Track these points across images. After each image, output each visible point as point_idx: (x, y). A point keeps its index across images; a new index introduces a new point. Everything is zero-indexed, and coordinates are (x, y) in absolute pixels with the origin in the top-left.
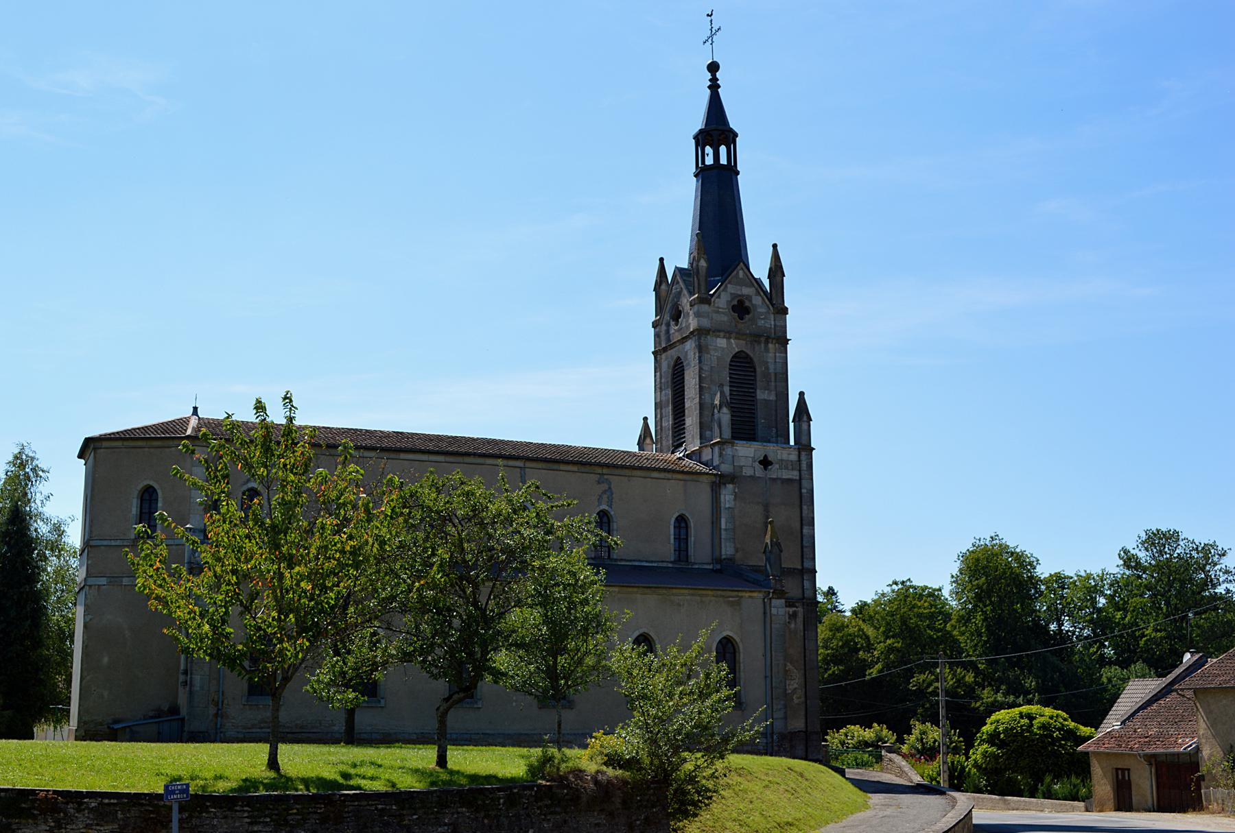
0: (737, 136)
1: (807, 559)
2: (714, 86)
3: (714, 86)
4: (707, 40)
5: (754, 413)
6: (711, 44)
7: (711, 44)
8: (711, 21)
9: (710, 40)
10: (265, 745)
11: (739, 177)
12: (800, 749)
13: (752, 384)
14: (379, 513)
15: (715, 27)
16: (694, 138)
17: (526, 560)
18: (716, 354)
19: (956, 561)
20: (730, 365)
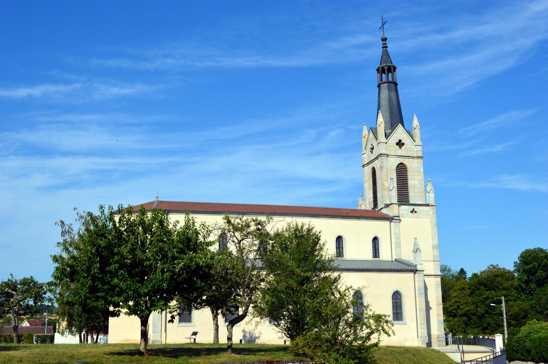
0: (396, 68)
1: (100, 217)
2: (385, 47)
3: (385, 47)
4: (381, 27)
5: (408, 194)
6: (383, 29)
7: (383, 29)
8: (382, 19)
9: (382, 27)
10: (168, 343)
11: (398, 86)
12: (396, 320)
13: (399, 188)
14: (456, 309)
15: (384, 21)
16: (377, 70)
17: (71, 241)
18: (389, 165)
19: (78, 214)
20: (396, 170)
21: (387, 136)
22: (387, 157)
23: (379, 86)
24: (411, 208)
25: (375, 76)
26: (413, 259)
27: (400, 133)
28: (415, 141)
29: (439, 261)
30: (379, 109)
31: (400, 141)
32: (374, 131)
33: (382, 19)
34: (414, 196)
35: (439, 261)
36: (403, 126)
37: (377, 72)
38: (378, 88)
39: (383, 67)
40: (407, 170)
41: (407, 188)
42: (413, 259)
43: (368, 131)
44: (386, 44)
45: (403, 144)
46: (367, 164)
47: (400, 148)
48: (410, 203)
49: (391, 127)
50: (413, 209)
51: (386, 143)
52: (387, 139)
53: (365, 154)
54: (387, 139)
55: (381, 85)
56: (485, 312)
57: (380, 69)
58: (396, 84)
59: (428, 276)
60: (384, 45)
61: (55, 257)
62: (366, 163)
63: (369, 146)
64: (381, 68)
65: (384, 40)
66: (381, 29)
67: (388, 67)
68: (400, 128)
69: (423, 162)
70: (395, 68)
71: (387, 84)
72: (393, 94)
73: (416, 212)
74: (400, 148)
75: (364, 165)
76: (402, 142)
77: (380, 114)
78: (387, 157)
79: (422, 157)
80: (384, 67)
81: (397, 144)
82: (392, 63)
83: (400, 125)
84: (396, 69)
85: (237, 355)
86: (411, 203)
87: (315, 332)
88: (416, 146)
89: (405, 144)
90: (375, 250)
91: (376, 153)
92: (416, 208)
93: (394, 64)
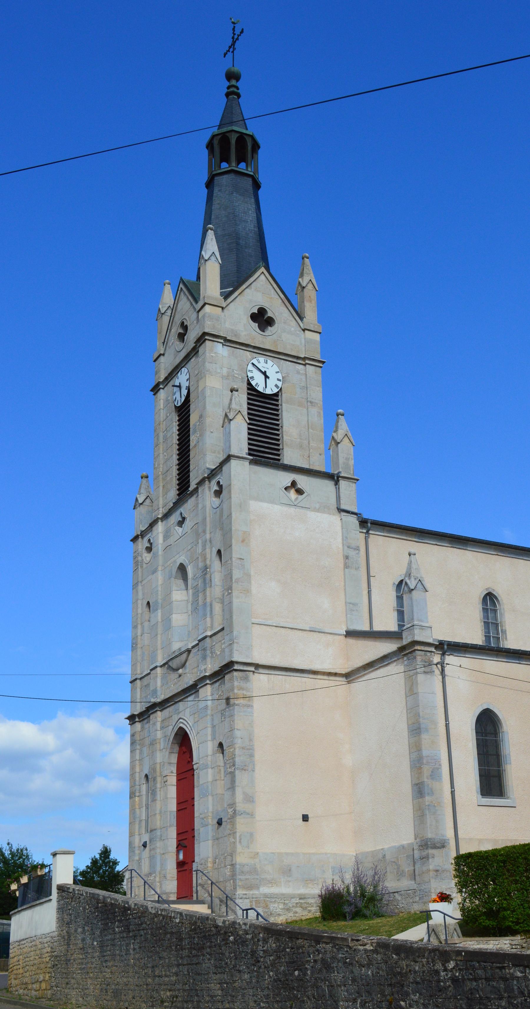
5: (278, 410)
6: (233, 52)
15: (237, 32)
23: (210, 184)
24: (287, 478)
29: (320, 333)
30: (208, 219)
35: (320, 333)
37: (206, 152)
38: (225, 99)
43: (173, 295)
44: (238, 89)
48: (281, 462)
51: (223, 308)
53: (162, 357)
57: (216, 142)
58: (257, 185)
62: (161, 380)
64: (220, 136)
65: (232, 76)
67: (187, 652)
69: (322, 371)
73: (300, 492)
75: (158, 385)
76: (266, 317)
77: (211, 235)
79: (323, 362)
80: (227, 134)
81: (254, 317)
83: (263, 269)
86: (286, 462)
88: (304, 330)
91: (192, 336)
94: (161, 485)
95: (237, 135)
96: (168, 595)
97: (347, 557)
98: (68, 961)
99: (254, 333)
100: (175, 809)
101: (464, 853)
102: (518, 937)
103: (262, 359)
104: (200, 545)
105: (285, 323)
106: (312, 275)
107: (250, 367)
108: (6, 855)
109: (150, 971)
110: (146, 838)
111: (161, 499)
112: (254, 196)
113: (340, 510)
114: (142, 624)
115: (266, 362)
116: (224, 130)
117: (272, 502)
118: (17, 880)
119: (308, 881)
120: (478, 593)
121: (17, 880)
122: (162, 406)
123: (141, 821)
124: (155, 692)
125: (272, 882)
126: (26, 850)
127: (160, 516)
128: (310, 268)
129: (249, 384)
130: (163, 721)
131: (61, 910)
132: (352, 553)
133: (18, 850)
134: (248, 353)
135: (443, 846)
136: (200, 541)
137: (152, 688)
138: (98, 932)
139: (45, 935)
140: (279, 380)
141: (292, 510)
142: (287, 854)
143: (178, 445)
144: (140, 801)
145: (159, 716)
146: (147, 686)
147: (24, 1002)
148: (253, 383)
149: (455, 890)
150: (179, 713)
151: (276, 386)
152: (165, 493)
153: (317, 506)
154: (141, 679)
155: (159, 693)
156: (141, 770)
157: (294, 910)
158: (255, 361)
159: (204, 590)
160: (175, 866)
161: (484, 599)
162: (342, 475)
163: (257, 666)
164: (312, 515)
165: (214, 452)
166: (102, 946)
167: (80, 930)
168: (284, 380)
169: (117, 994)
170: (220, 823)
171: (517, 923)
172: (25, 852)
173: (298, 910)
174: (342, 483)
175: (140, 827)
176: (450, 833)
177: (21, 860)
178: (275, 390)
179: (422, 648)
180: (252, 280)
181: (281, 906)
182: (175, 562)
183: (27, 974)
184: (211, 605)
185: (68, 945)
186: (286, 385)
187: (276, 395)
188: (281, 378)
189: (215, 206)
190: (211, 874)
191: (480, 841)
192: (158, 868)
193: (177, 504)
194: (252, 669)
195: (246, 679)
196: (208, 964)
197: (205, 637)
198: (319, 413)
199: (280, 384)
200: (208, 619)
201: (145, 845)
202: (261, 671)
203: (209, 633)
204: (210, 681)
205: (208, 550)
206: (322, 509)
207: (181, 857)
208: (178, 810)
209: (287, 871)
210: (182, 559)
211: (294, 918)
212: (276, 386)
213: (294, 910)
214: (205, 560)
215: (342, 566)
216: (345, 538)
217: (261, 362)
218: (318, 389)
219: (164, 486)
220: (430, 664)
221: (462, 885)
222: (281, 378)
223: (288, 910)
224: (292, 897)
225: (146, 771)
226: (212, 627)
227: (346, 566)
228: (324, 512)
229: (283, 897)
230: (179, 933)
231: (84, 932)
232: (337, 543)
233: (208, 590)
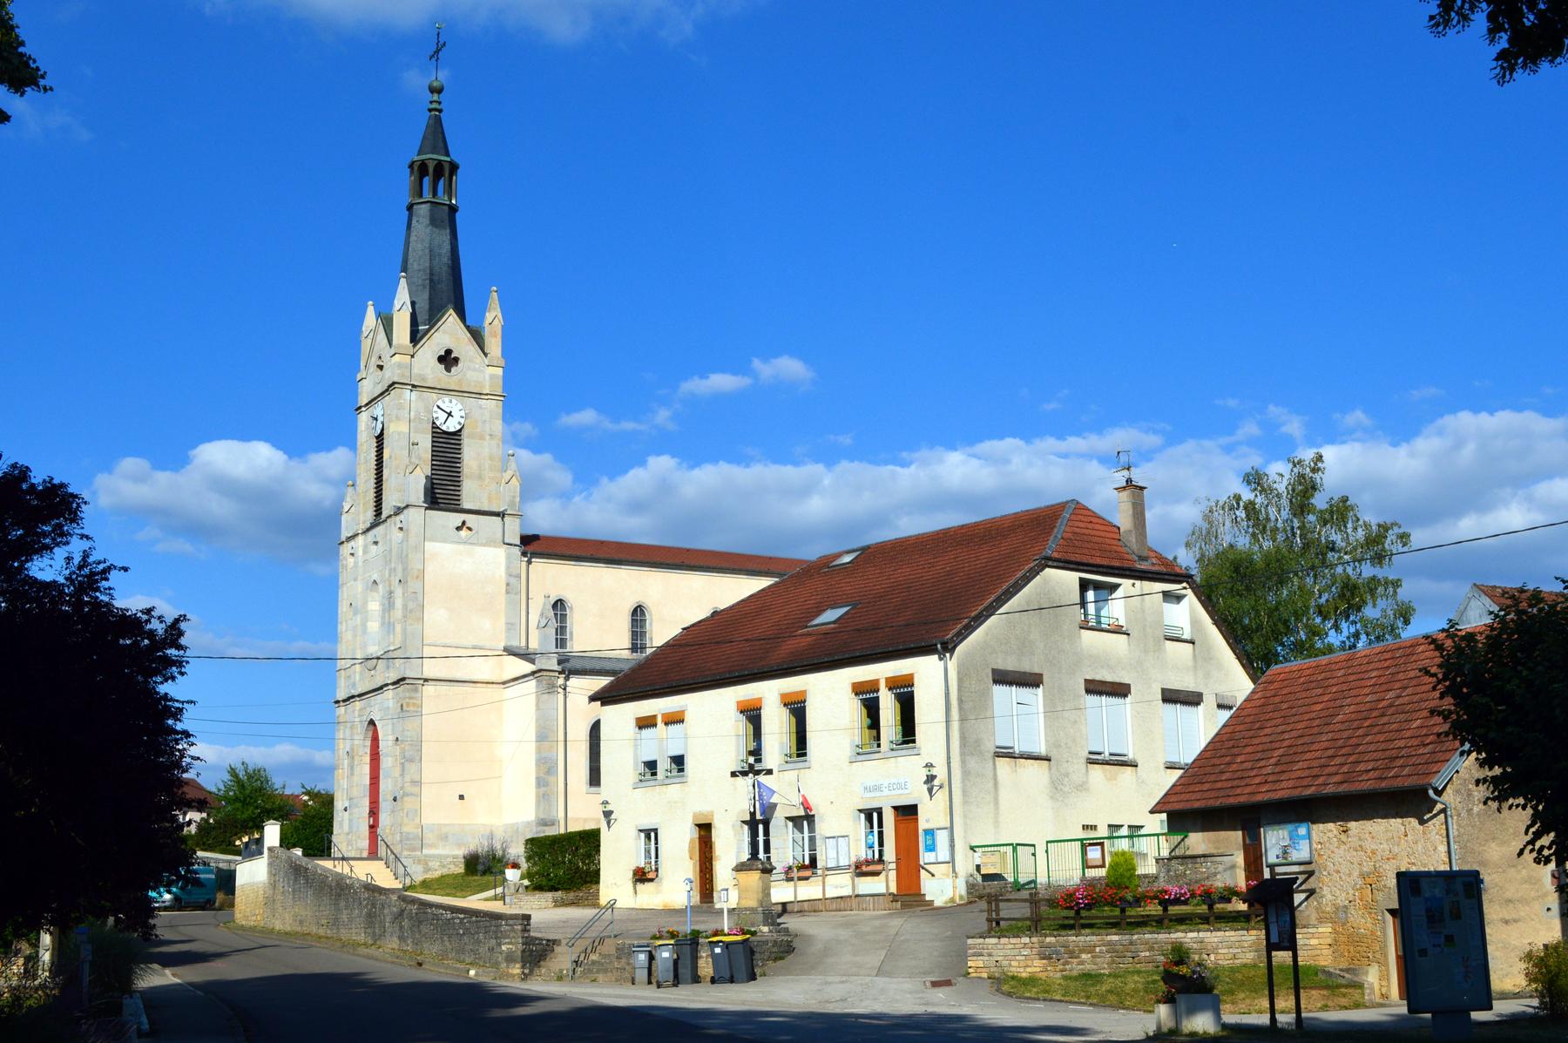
0: (458, 168)
6: (439, 42)
11: (457, 214)
16: (409, 167)
21: (415, 338)
22: (411, 391)
23: (410, 208)
25: (406, 179)
26: (719, 889)
27: (450, 332)
28: (486, 355)
31: (449, 352)
32: (387, 323)
33: (438, 34)
34: (471, 493)
36: (462, 315)
39: (423, 160)
40: (460, 449)
41: (458, 503)
42: (719, 889)
45: (456, 360)
46: (367, 405)
47: (448, 370)
49: (430, 316)
50: (464, 523)
52: (414, 346)
54: (414, 346)
55: (415, 207)
56: (1208, 987)
59: (484, 685)
60: (434, 106)
61: (1237, 570)
63: (374, 361)
66: (434, 59)
68: (451, 318)
70: (454, 168)
71: (429, 204)
72: (445, 237)
74: (448, 370)
78: (411, 391)
81: (441, 359)
82: (447, 154)
84: (459, 171)
85: (252, 748)
87: (1514, 47)
89: (444, 110)
90: (1224, 918)
92: (470, 519)
93: (455, 156)
94: (362, 502)
95: (436, 162)
96: (365, 603)
97: (508, 585)
98: (274, 900)
99: (441, 374)
100: (368, 783)
101: (573, 830)
102: (560, 892)
103: (447, 399)
104: (387, 572)
105: (470, 361)
106: (499, 310)
107: (436, 409)
108: (241, 776)
109: (317, 908)
110: (347, 805)
111: (361, 515)
112: (450, 226)
113: (504, 544)
114: (346, 621)
115: (451, 402)
116: (424, 157)
117: (444, 541)
118: (240, 839)
119: (459, 845)
120: (631, 606)
121: (240, 839)
122: (363, 429)
123: (343, 789)
124: (354, 685)
125: (431, 846)
126: (265, 771)
127: (360, 532)
128: (497, 302)
129: (434, 423)
130: (360, 710)
131: (270, 864)
132: (513, 581)
133: (254, 771)
134: (434, 395)
135: (553, 824)
136: (387, 568)
137: (352, 681)
138: (291, 882)
139: (260, 882)
140: (462, 417)
141: (461, 547)
142: (444, 825)
143: (376, 474)
144: (343, 772)
145: (358, 704)
146: (349, 677)
147: (1088, 967)
148: (438, 423)
149: (524, 860)
150: (371, 706)
151: (460, 423)
152: (365, 512)
153: (484, 541)
154: (345, 669)
155: (357, 686)
156: (344, 748)
157: (448, 866)
158: (440, 403)
159: (389, 611)
160: (368, 828)
161: (635, 612)
162: (508, 512)
163: (426, 680)
164: (480, 550)
165: (400, 491)
166: (294, 891)
167: (281, 880)
168: (466, 417)
169: (301, 922)
170: (395, 800)
171: (559, 884)
172: (262, 773)
173: (452, 866)
174: (506, 518)
175: (343, 795)
176: (561, 814)
177: (259, 782)
178: (458, 427)
179: (548, 673)
180: (440, 323)
181: (438, 864)
182: (370, 576)
183: (248, 910)
184: (394, 625)
185: (274, 889)
186: (468, 421)
187: (460, 430)
188: (464, 415)
189: (413, 238)
190: (389, 838)
191: (585, 820)
192: (355, 830)
193: (373, 526)
194: (421, 682)
195: (416, 690)
196: (342, 904)
197: (389, 651)
198: (499, 445)
199: (462, 421)
200: (392, 636)
201: (345, 810)
202: (430, 683)
203: (392, 648)
204: (1046, 581)
205: (392, 578)
206: (490, 543)
207: (371, 822)
208: (371, 784)
209: (444, 838)
210: (375, 577)
211: (448, 873)
212: (460, 423)
213: (448, 866)
214: (390, 585)
215: (504, 590)
216: (508, 568)
217: (447, 403)
218: (497, 421)
219: (364, 504)
220: (554, 686)
221: (528, 859)
222: (464, 415)
223: (444, 866)
224: (448, 856)
225: (348, 749)
226: (393, 643)
227: (507, 592)
228: (490, 546)
229: (440, 856)
230: (331, 886)
231: (284, 881)
232: (501, 573)
233: (392, 611)
